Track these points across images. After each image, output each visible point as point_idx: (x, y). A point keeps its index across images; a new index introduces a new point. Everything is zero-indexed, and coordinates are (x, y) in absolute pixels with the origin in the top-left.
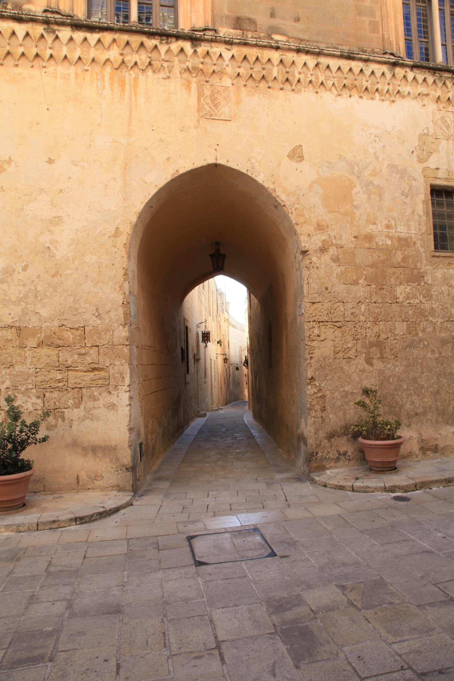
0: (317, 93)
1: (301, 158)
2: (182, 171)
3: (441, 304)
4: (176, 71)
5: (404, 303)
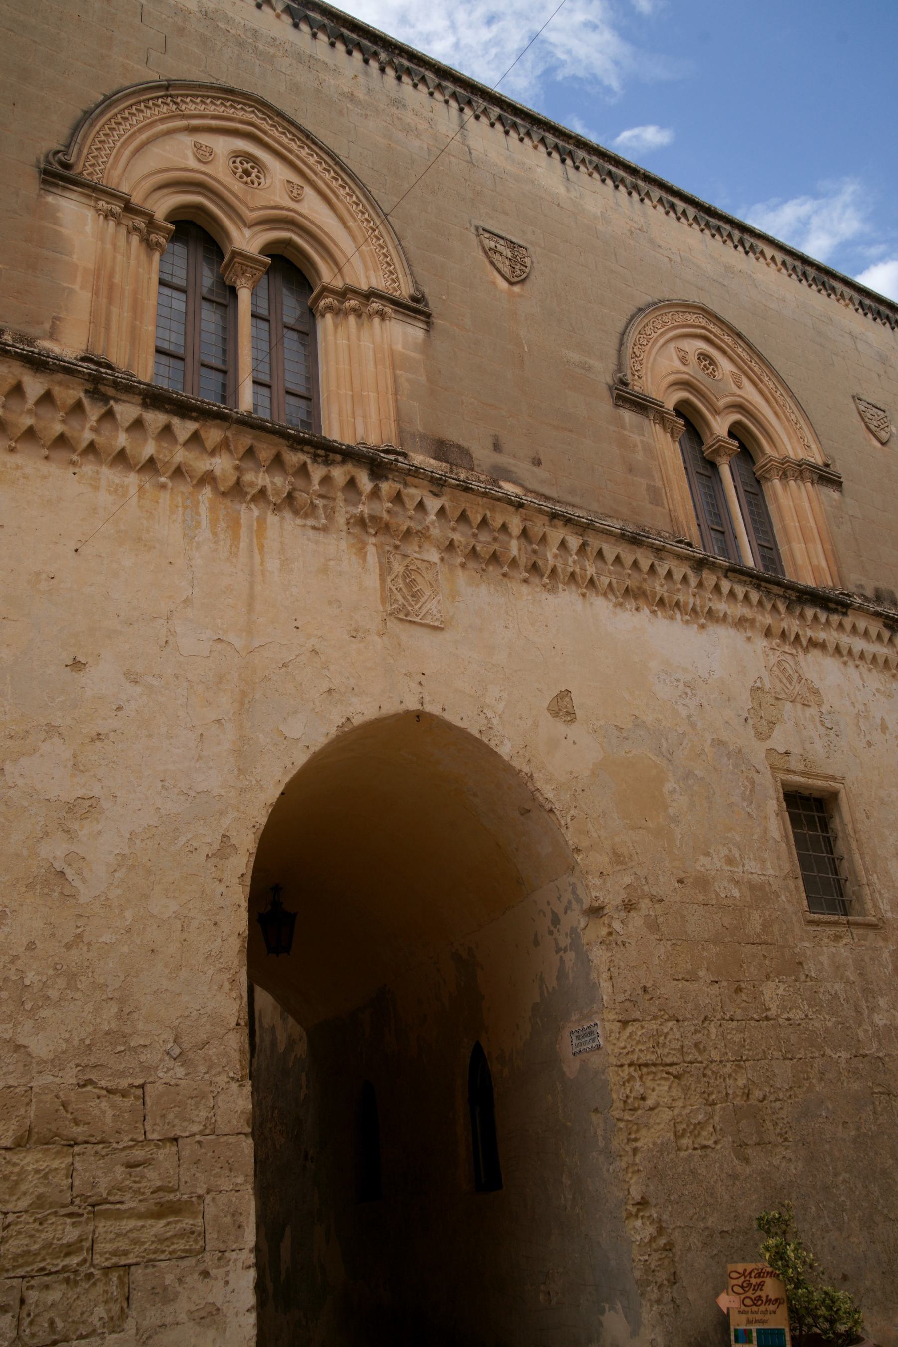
0: (584, 595)
1: (570, 716)
2: (357, 721)
3: (840, 1019)
4: (341, 520)
5: (780, 1019)
